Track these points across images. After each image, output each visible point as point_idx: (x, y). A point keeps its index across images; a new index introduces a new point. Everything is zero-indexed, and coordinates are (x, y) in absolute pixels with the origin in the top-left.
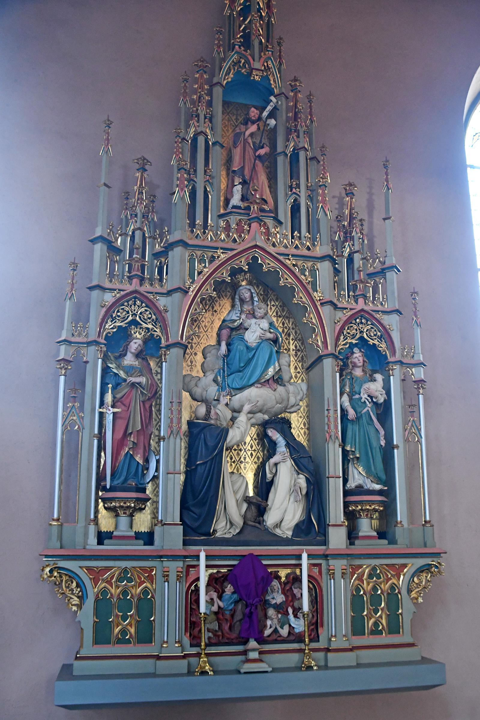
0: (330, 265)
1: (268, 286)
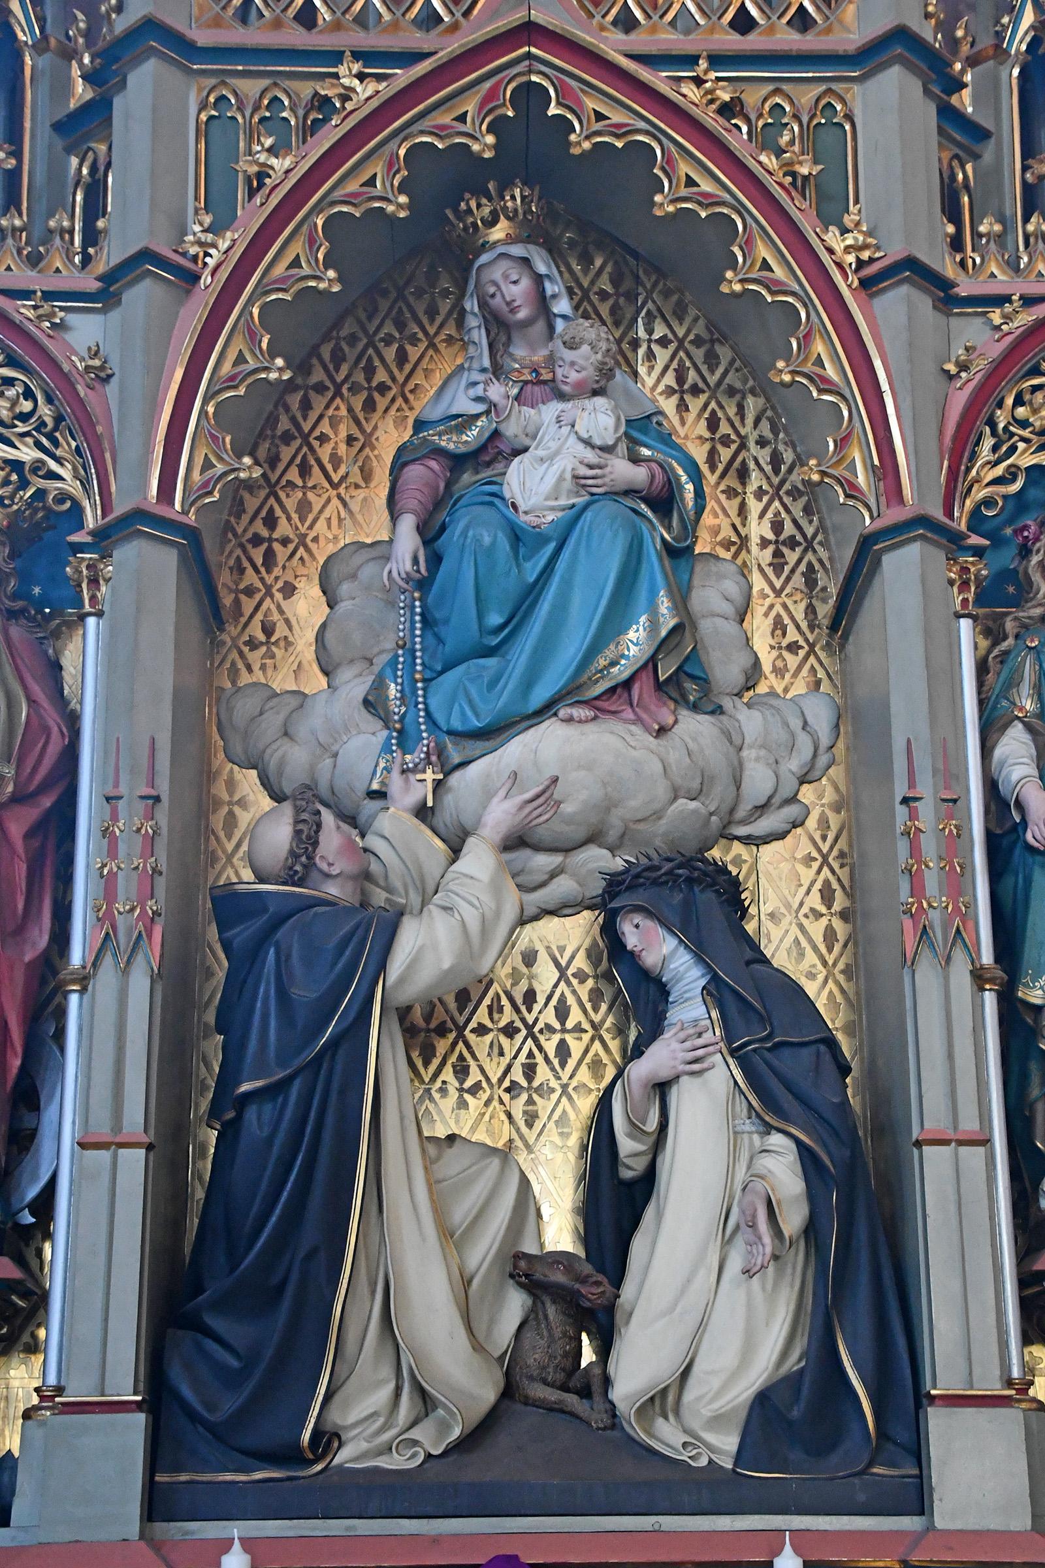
0: (915, 86)
1: (636, 255)
